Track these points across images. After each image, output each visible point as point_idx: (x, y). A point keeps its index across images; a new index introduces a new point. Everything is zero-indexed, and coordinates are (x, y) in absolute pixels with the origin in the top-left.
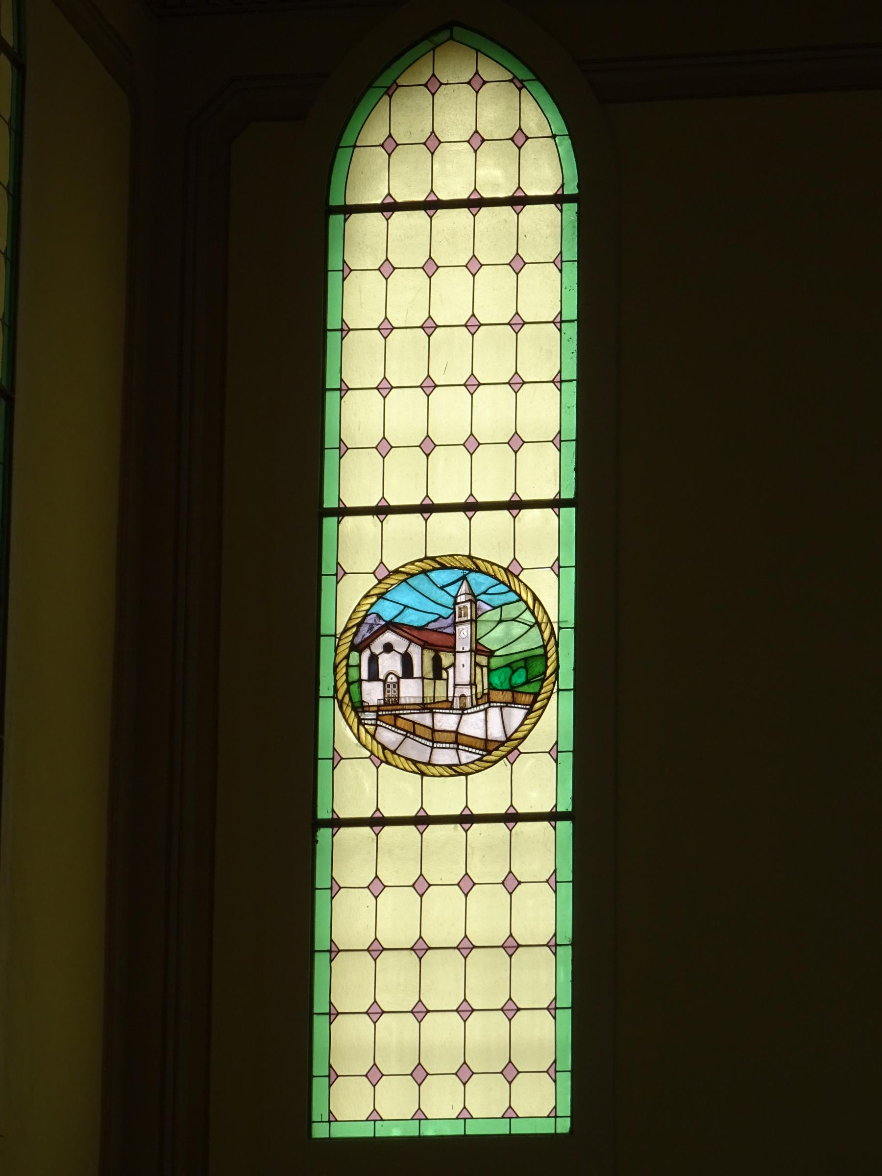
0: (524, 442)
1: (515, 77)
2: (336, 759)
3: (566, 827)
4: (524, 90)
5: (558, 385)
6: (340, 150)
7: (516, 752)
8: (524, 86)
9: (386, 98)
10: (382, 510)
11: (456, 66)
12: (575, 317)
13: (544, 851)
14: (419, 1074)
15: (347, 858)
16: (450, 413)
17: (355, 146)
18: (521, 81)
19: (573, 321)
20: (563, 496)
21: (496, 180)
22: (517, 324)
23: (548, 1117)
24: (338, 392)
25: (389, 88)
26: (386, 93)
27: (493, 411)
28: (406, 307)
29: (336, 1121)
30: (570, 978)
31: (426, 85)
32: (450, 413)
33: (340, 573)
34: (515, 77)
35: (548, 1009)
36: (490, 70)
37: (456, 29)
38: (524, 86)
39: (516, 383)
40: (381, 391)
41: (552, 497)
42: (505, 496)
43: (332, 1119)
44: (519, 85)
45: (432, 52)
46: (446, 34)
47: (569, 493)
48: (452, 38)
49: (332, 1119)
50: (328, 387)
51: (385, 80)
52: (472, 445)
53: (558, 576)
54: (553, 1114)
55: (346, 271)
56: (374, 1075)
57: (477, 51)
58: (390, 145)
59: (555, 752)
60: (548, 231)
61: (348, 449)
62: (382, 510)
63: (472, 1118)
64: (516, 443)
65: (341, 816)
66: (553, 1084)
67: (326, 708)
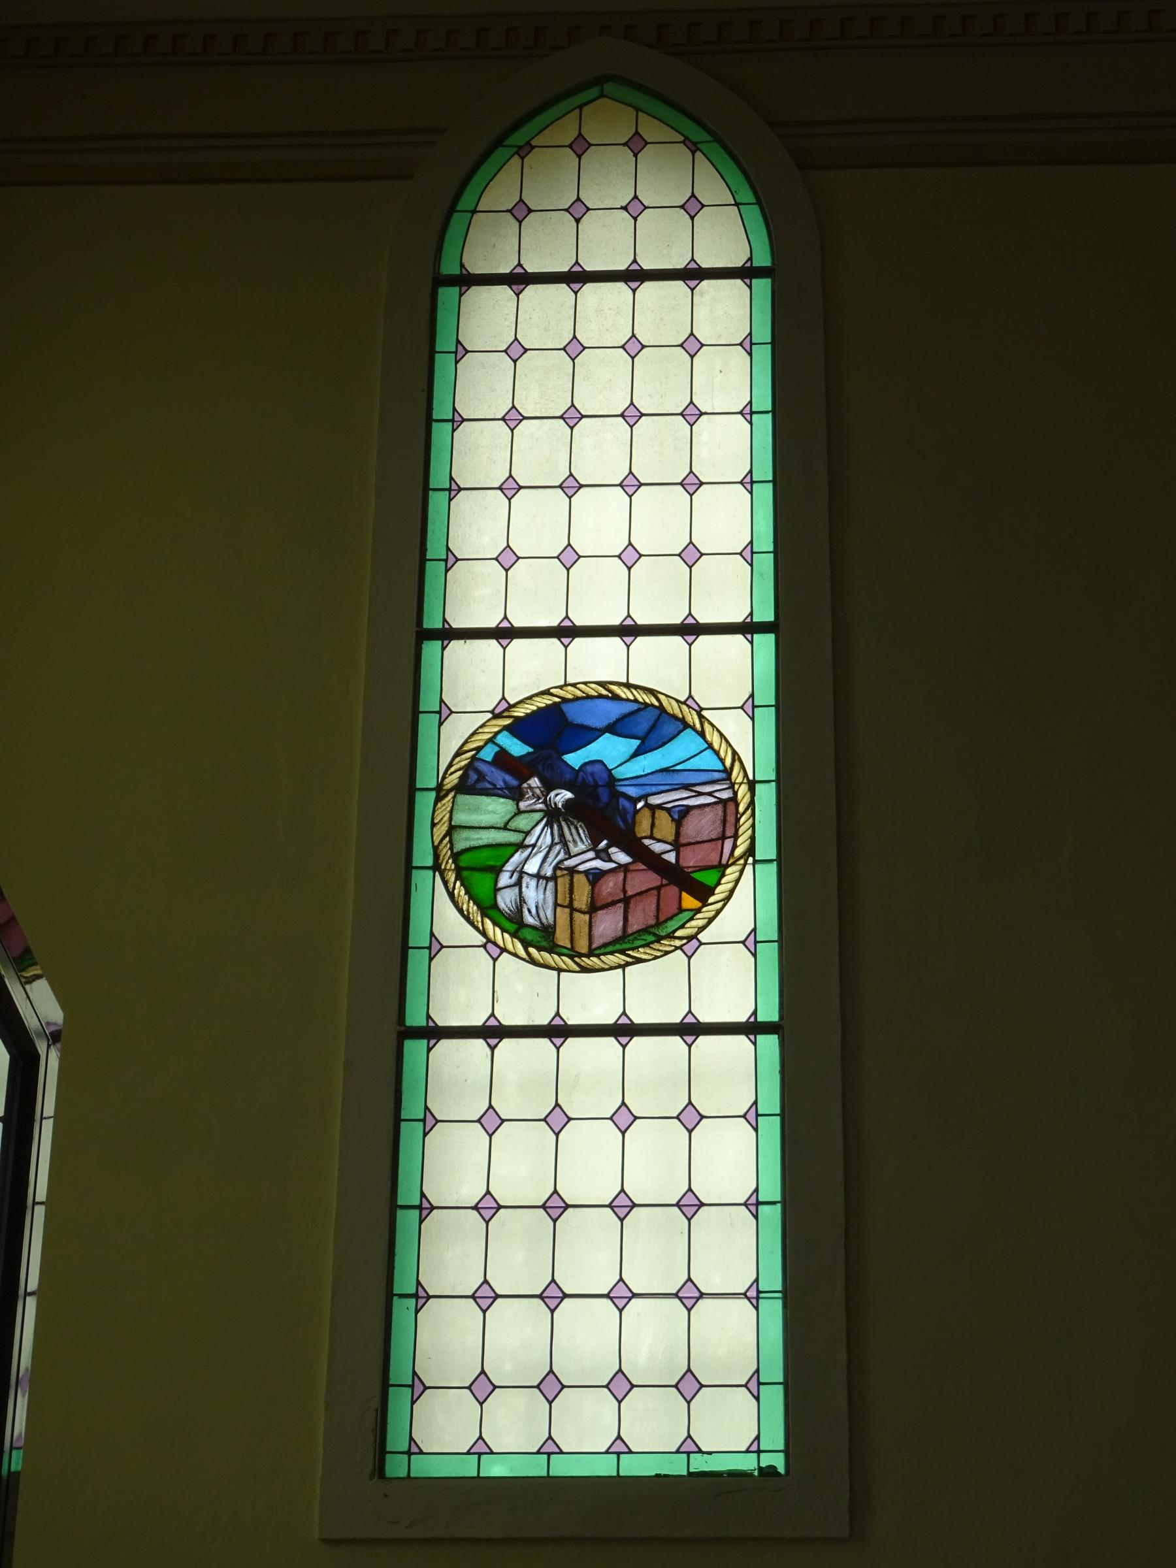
0: (702, 1386)
1: (686, 138)
2: (750, 707)
3: (766, 643)
4: (698, 154)
5: (753, 1209)
6: (456, 215)
7: (694, 943)
8: (698, 149)
9: (516, 158)
10: (505, 633)
11: (608, 120)
12: (778, 1197)
13: (739, 1072)
14: (550, 1386)
15: (453, 1075)
16: (600, 521)
17: (474, 212)
18: (695, 144)
19: (771, 861)
20: (761, 1018)
21: (664, 245)
22: (690, 1205)
23: (748, 1451)
24: (417, 1212)
25: (520, 148)
26: (517, 153)
27: (660, 520)
28: (517, 1261)
29: (421, 1452)
30: (773, 765)
31: (570, 146)
32: (587, 1337)
33: (443, 713)
34: (686, 138)
35: (745, 1204)
36: (651, 129)
37: (609, 88)
38: (698, 149)
39: (692, 484)
40: (482, 1211)
41: (740, 620)
42: (676, 617)
43: (413, 1450)
44: (693, 148)
45: (577, 111)
46: (594, 92)
47: (770, 1013)
48: (601, 96)
49: (414, 1449)
50: (391, 1382)
51: (518, 138)
52: (630, 556)
53: (753, 719)
54: (754, 1448)
55: (460, 351)
56: (482, 1387)
57: (638, 110)
58: (521, 212)
59: (752, 942)
60: (731, 312)
61: (437, 1121)
62: (505, 633)
63: (630, 1452)
64: (691, 555)
65: (440, 1024)
66: (755, 1403)
67: (766, 768)
